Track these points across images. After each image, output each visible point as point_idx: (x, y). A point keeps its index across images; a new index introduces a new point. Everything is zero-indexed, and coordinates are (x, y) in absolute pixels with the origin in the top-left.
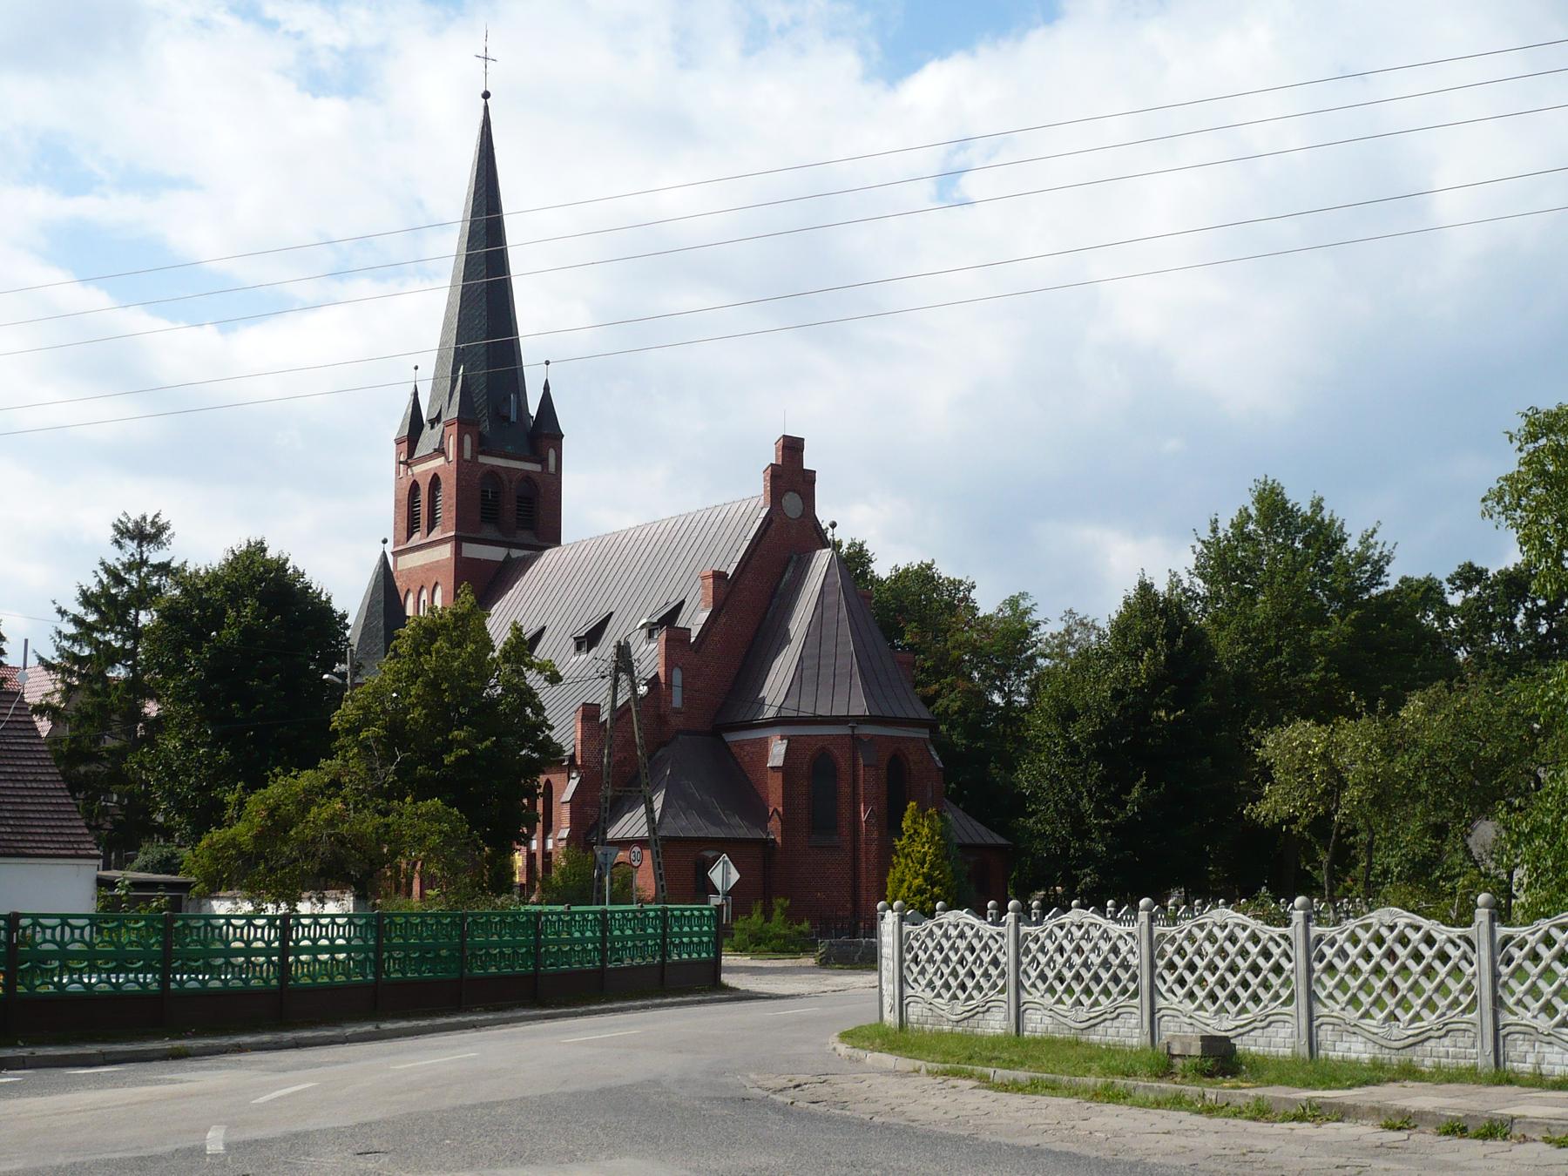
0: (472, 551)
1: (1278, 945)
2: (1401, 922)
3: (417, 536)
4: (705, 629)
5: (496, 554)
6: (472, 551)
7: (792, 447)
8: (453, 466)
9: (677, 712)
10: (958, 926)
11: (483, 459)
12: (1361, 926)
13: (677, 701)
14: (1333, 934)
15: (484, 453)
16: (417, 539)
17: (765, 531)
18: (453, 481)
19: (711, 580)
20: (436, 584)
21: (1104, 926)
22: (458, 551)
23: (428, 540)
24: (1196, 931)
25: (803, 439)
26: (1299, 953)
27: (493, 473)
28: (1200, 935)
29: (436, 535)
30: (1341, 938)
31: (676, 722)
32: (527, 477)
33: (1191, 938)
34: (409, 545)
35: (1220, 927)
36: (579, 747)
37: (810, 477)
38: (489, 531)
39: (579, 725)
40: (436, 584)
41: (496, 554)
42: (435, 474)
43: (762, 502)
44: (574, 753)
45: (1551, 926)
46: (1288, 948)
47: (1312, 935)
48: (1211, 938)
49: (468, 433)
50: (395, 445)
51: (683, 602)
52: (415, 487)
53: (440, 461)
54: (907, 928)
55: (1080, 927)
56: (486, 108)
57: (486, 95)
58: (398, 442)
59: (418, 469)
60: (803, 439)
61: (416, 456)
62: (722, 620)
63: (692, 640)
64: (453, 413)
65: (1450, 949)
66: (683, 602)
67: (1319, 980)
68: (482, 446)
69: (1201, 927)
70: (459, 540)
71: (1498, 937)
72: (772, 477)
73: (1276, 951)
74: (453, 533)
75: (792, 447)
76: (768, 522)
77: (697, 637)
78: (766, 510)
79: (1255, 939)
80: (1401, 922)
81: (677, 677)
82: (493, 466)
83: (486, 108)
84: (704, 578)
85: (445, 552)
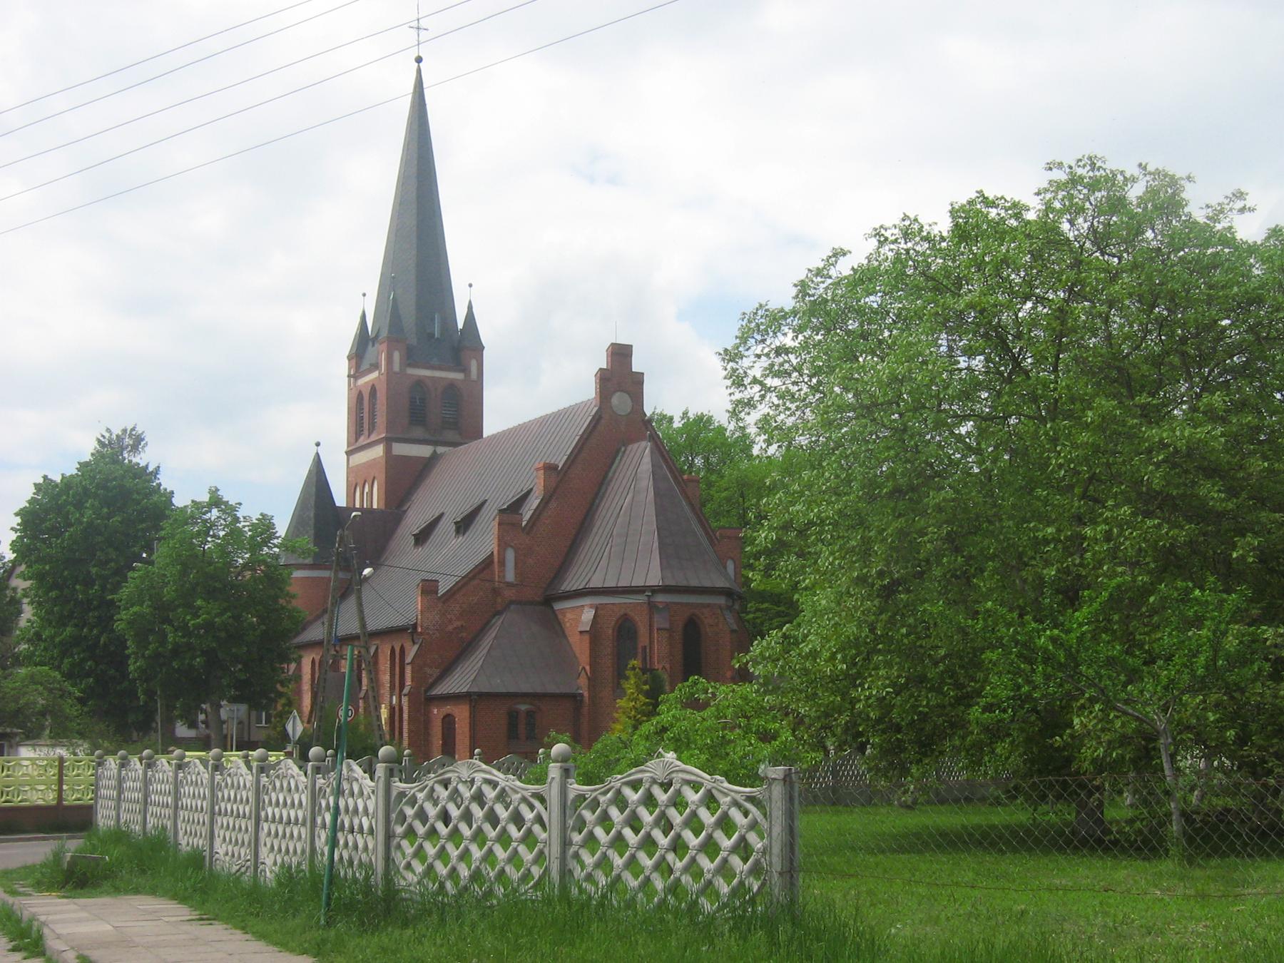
0: (401, 449)
1: (532, 807)
2: (479, 777)
3: (362, 438)
4: (537, 513)
5: (424, 451)
6: (401, 449)
7: (621, 354)
8: (384, 378)
9: (509, 585)
10: (670, 784)
11: (411, 371)
12: (629, 784)
13: (510, 576)
14: (594, 794)
15: (410, 365)
16: (363, 441)
17: (595, 427)
18: (384, 391)
19: (542, 471)
20: (374, 478)
21: (708, 785)
22: (388, 451)
23: (369, 441)
24: (627, 791)
25: (632, 346)
26: (553, 815)
27: (419, 383)
28: (632, 796)
29: (374, 437)
30: (420, 796)
31: (509, 594)
32: (451, 386)
33: (621, 802)
34: (358, 444)
35: (662, 785)
36: (419, 617)
37: (638, 380)
38: (418, 432)
39: (420, 598)
40: (374, 478)
41: (424, 451)
42: (373, 385)
43: (594, 403)
44: (416, 623)
45: (436, 782)
46: (760, 817)
47: (571, 796)
48: (649, 801)
49: (397, 349)
50: (347, 361)
51: (532, 489)
52: (360, 397)
53: (375, 375)
54: (399, 785)
55: (666, 786)
56: (419, 71)
57: (419, 60)
58: (350, 358)
59: (361, 381)
60: (632, 346)
61: (361, 370)
62: (553, 505)
63: (524, 523)
64: (384, 333)
65: (735, 814)
66: (532, 489)
67: (576, 856)
68: (411, 358)
69: (635, 785)
70: (388, 441)
71: (571, 796)
72: (601, 379)
73: (529, 815)
74: (384, 435)
75: (621, 354)
76: (597, 420)
77: (528, 522)
78: (596, 409)
79: (710, 801)
80: (479, 777)
81: (510, 555)
82: (419, 376)
83: (419, 71)
84: (538, 469)
85: (378, 451)
